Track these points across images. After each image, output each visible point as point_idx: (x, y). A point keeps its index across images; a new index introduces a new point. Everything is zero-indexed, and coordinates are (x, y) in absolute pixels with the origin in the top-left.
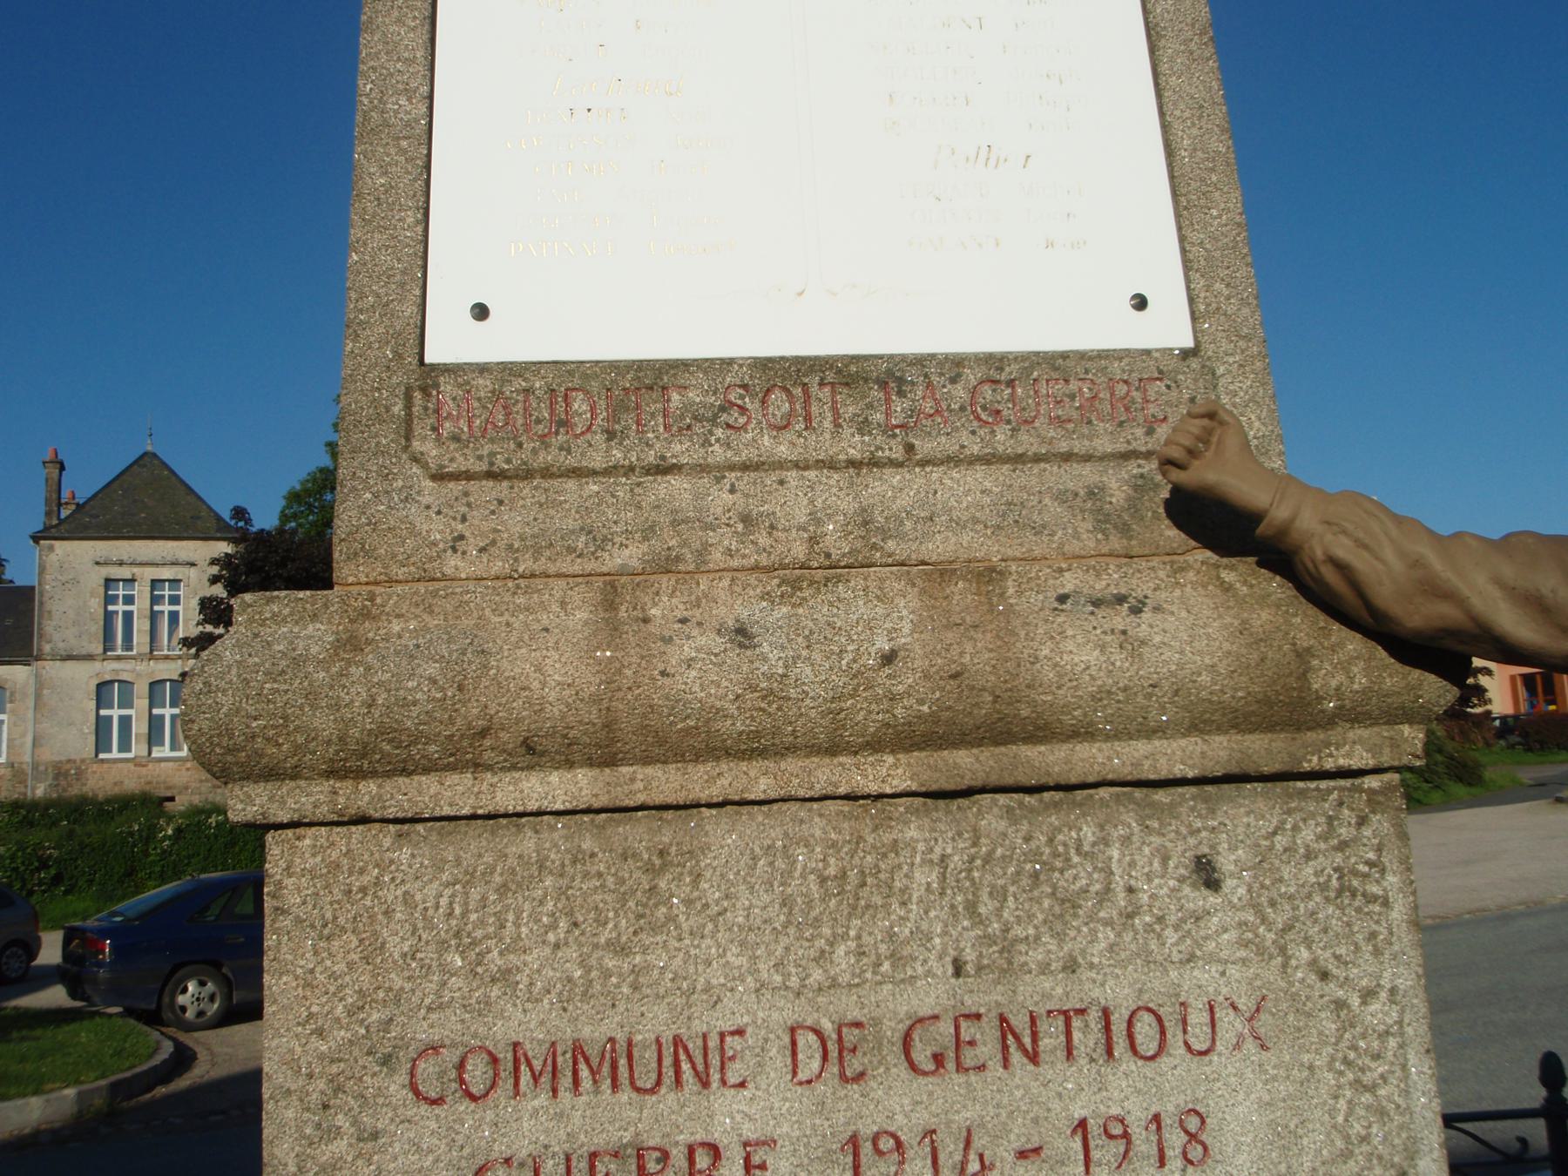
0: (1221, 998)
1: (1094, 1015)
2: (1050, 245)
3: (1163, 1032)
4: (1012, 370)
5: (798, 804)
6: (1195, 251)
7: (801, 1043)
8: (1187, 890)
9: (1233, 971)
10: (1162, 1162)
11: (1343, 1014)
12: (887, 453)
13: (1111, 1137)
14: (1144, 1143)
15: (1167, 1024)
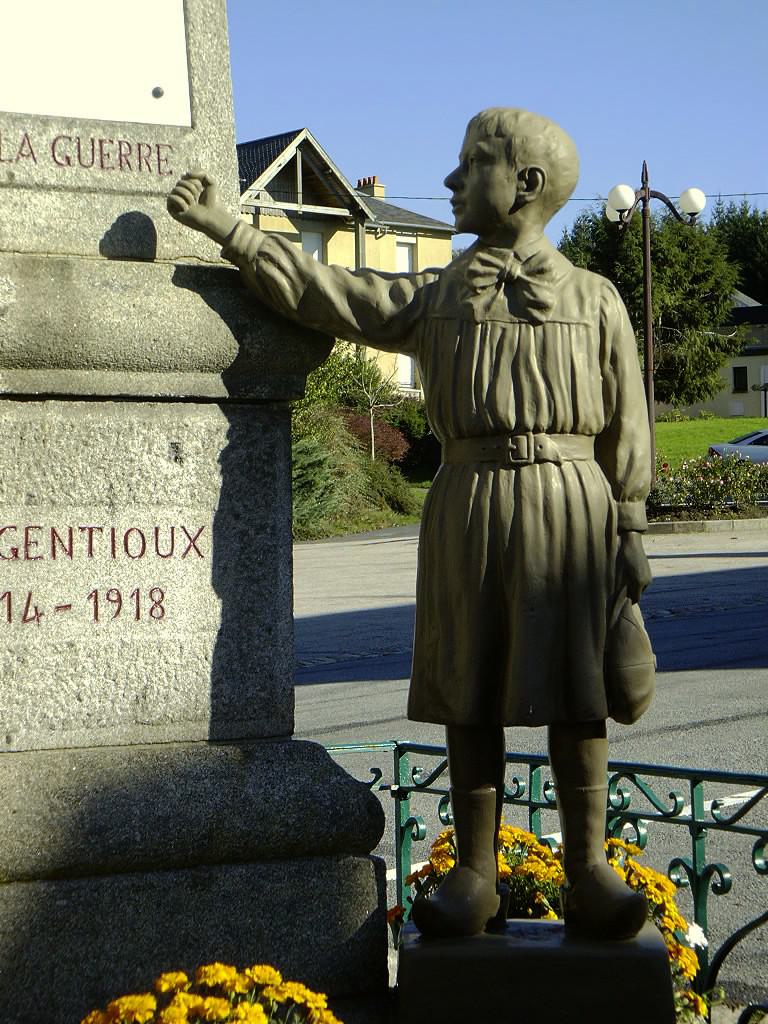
0: (178, 526)
1: (107, 530)
3: (144, 544)
6: (195, 62)
9: (188, 512)
10: (138, 617)
11: (246, 538)
13: (112, 601)
14: (129, 606)
15: (146, 539)
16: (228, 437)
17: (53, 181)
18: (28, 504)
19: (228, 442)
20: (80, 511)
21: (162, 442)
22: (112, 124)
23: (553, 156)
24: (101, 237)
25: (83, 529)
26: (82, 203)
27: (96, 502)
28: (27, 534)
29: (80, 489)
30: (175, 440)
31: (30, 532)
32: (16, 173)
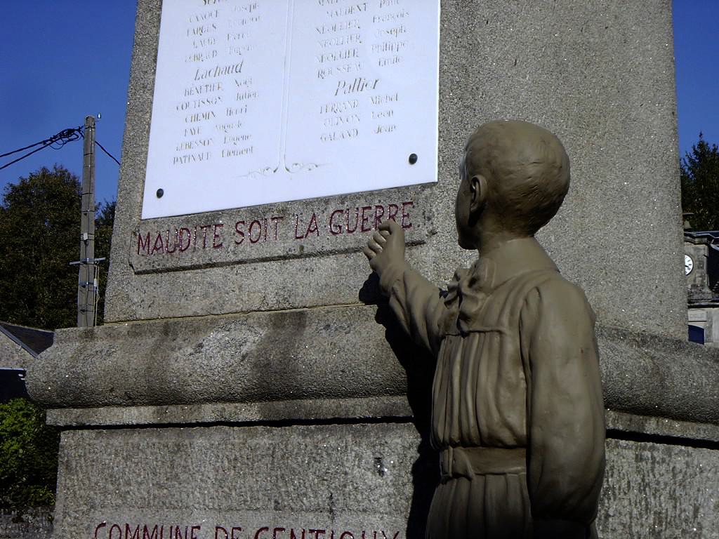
2: (379, 130)
4: (412, 194)
5: (93, 433)
7: (219, 534)
8: (369, 474)
12: (293, 252)
16: (419, 451)
17: (328, 248)
18: (276, 509)
19: (418, 455)
20: (311, 516)
21: (369, 456)
22: (371, 193)
23: (493, 163)
24: (361, 287)
25: (312, 531)
26: (350, 261)
27: (319, 509)
28: (275, 533)
29: (310, 497)
30: (379, 456)
31: (277, 532)
32: (305, 245)
